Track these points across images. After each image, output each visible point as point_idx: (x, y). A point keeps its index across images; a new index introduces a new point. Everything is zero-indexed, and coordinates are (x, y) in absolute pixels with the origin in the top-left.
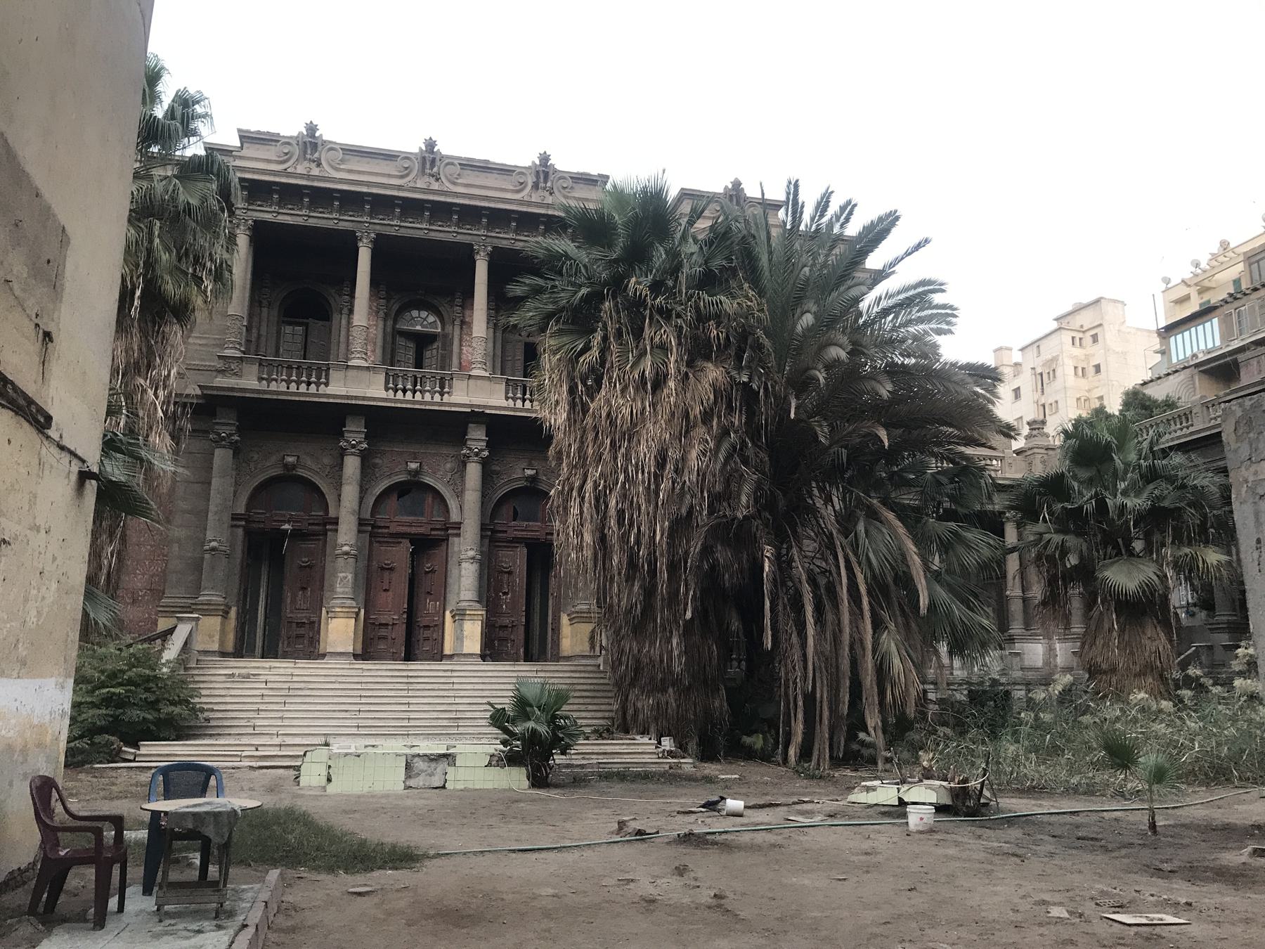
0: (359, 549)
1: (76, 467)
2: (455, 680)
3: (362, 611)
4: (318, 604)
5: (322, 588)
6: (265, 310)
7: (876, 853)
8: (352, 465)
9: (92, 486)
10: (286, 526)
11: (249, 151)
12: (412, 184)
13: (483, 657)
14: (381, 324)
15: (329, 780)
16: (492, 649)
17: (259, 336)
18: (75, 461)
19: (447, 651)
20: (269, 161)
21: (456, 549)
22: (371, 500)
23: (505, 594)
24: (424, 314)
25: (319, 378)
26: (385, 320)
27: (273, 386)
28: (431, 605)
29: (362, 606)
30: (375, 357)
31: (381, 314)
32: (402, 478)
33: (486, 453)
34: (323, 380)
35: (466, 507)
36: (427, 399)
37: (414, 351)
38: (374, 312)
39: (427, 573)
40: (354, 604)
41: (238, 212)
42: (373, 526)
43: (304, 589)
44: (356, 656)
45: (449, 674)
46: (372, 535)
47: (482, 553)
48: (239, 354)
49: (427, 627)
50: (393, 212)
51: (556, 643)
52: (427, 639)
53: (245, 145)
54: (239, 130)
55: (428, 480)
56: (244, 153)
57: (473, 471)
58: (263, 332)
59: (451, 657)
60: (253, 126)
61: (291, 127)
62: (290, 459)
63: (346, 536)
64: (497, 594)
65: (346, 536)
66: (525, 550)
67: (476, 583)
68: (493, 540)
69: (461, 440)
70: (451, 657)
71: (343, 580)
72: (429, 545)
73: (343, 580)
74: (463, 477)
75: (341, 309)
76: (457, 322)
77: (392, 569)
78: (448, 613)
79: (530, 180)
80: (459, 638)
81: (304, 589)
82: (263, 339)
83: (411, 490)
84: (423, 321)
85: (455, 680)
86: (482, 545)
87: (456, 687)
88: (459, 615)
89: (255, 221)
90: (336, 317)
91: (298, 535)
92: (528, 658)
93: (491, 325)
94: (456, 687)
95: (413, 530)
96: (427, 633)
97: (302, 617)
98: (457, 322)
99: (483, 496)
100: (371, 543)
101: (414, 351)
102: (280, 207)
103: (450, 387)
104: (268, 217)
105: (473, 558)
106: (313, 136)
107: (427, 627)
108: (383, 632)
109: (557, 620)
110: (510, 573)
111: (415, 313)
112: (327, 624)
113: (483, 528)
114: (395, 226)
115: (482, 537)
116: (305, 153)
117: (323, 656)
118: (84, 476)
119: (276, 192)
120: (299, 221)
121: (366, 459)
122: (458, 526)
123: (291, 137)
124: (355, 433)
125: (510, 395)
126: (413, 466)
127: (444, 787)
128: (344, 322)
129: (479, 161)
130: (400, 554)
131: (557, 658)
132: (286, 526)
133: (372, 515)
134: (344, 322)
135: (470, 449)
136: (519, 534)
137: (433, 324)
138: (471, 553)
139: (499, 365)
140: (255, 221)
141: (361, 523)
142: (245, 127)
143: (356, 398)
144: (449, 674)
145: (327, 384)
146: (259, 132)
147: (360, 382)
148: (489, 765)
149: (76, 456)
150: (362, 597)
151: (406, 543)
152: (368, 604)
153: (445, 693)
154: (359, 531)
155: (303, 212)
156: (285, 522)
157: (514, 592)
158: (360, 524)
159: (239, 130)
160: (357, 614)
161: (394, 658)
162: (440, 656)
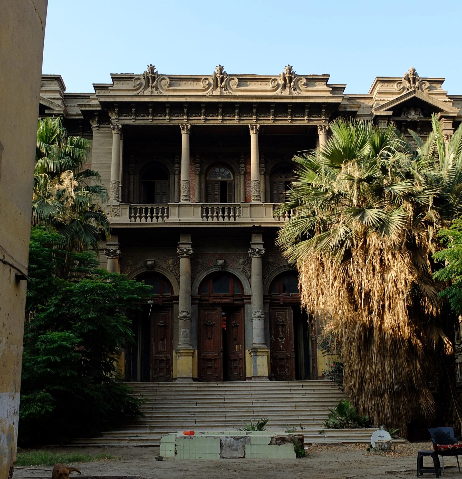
0: (192, 314)
1: (14, 272)
2: (253, 392)
3: (197, 351)
4: (170, 348)
5: (172, 339)
6: (132, 176)
7: (188, 471)
8: (184, 263)
9: (23, 283)
10: (150, 302)
11: (119, 85)
12: (211, 94)
13: (270, 378)
14: (197, 178)
15: (176, 453)
16: (276, 373)
17: (129, 192)
18: (13, 270)
19: (248, 375)
20: (128, 90)
21: (249, 311)
22: (197, 284)
23: (281, 338)
24: (223, 170)
25: (163, 213)
26: (200, 176)
27: (138, 220)
28: (237, 347)
29: (196, 348)
30: (195, 198)
31: (198, 173)
32: (214, 270)
33: (191, 251)
34: (165, 214)
35: (253, 285)
36: (227, 222)
37: (219, 193)
38: (191, 171)
39: (233, 327)
40: (191, 348)
41: (113, 121)
42: (200, 300)
43: (162, 340)
44: (194, 379)
45: (249, 389)
46: (200, 305)
47: (265, 313)
48: (118, 204)
49: (236, 360)
50: (165, 111)
51: (315, 368)
52: (236, 368)
53: (115, 83)
54: (111, 75)
55: (231, 270)
56: (115, 87)
57: (256, 263)
58: (132, 189)
59: (250, 378)
60: (118, 71)
61: (140, 69)
62: (149, 263)
63: (183, 307)
64: (276, 339)
65: (183, 307)
66: (292, 311)
67: (263, 333)
68: (271, 305)
69: (247, 245)
70: (250, 378)
71: (183, 335)
72: (235, 310)
73: (183, 335)
74: (250, 267)
75: (174, 172)
76: (242, 173)
77: (212, 326)
78: (247, 351)
79: (281, 82)
80: (255, 367)
81: (162, 340)
82: (132, 193)
83: (223, 278)
84: (222, 175)
85: (253, 392)
86: (264, 308)
87: (253, 396)
88: (255, 352)
89: (123, 126)
90: (171, 177)
91: (157, 308)
92: (298, 378)
93: (263, 173)
94: (253, 396)
95: (224, 301)
96: (236, 364)
97: (162, 356)
98: (242, 173)
99: (264, 278)
100: (199, 309)
101: (219, 193)
102: (153, 116)
103: (168, 213)
104: (130, 122)
105: (260, 317)
106: (152, 73)
107: (236, 360)
108: (209, 364)
109: (315, 353)
110: (283, 325)
111: (217, 170)
112: (176, 360)
113: (265, 298)
114: (269, 121)
115: (265, 303)
116: (149, 82)
117: (175, 379)
118: (19, 278)
119: (133, 107)
120: (148, 123)
121: (193, 260)
122: (249, 297)
123: (140, 75)
124: (185, 244)
125: (204, 214)
126: (220, 262)
127: (244, 457)
128: (176, 179)
129: (249, 75)
130: (217, 316)
131: (316, 377)
132: (150, 302)
133: (199, 293)
134: (176, 179)
135: (254, 249)
136: (287, 301)
137: (228, 176)
138: (258, 314)
139: (268, 196)
140: (123, 126)
141: (193, 298)
142: (114, 73)
143: (185, 223)
144: (249, 389)
145: (168, 217)
146: (122, 74)
147: (186, 212)
148: (271, 443)
149: (13, 267)
150: (195, 343)
151: (219, 309)
152: (200, 347)
153: (247, 401)
154: (192, 303)
155: (132, 117)
156: (149, 300)
157: (286, 337)
158: (192, 299)
159: (111, 75)
160: (193, 353)
161: (217, 379)
162: (244, 378)
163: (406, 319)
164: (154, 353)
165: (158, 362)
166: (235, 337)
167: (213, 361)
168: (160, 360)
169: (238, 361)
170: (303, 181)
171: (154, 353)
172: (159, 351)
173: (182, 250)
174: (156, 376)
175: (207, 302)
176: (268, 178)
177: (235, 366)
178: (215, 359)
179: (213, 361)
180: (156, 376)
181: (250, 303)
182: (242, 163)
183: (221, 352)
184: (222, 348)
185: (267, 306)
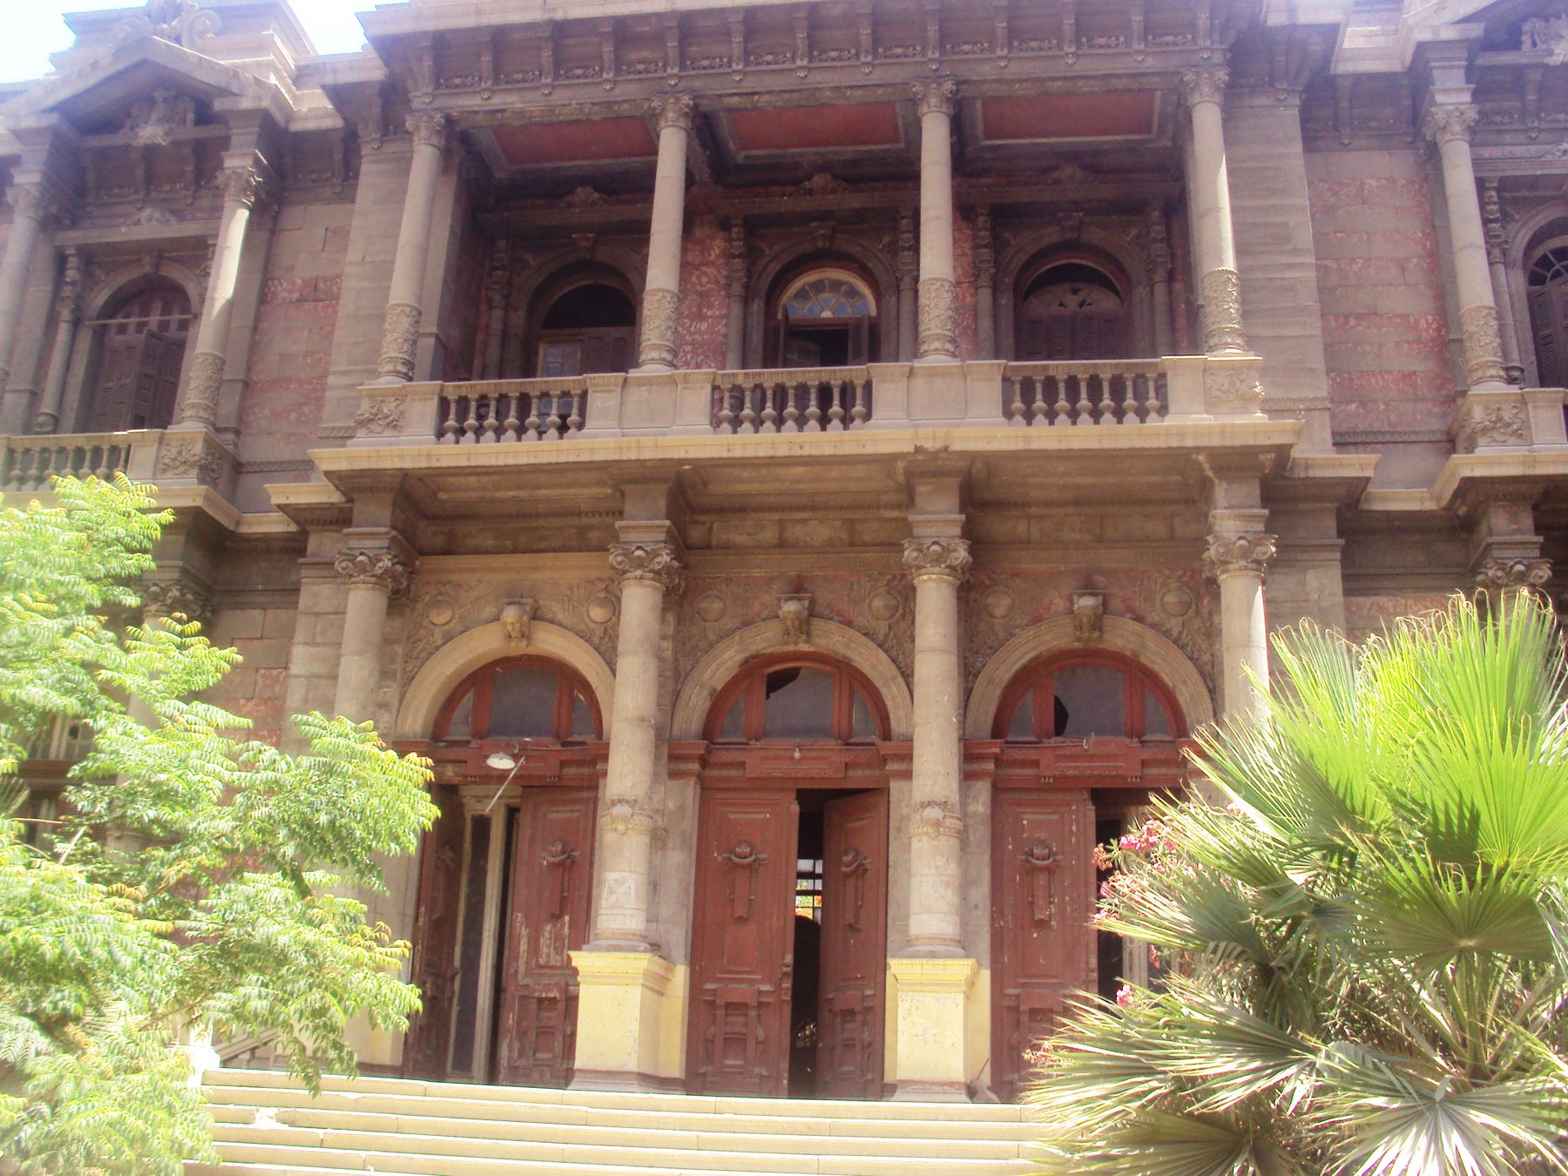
31: (737, 289)
39: (847, 876)
81: (556, 917)
93: (985, 280)
103: (582, 413)
125: (726, 412)
152: (705, 952)
158: (673, 758)
163: (47, 1041)
164: (522, 968)
165: (533, 1005)
166: (850, 918)
167: (753, 1013)
168: (540, 1001)
169: (859, 1018)
170: (1209, 838)
171: (522, 968)
172: (542, 961)
173: (627, 554)
174: (521, 1063)
175: (734, 773)
176: (1006, 300)
177: (846, 1035)
178: (761, 1005)
179: (753, 1013)
180: (521, 1063)
181: (908, 775)
182: (904, 249)
183: (785, 974)
184: (789, 959)
185: (983, 789)
